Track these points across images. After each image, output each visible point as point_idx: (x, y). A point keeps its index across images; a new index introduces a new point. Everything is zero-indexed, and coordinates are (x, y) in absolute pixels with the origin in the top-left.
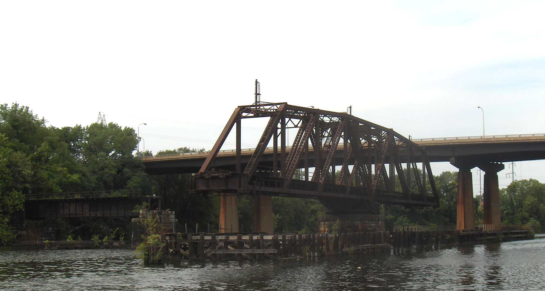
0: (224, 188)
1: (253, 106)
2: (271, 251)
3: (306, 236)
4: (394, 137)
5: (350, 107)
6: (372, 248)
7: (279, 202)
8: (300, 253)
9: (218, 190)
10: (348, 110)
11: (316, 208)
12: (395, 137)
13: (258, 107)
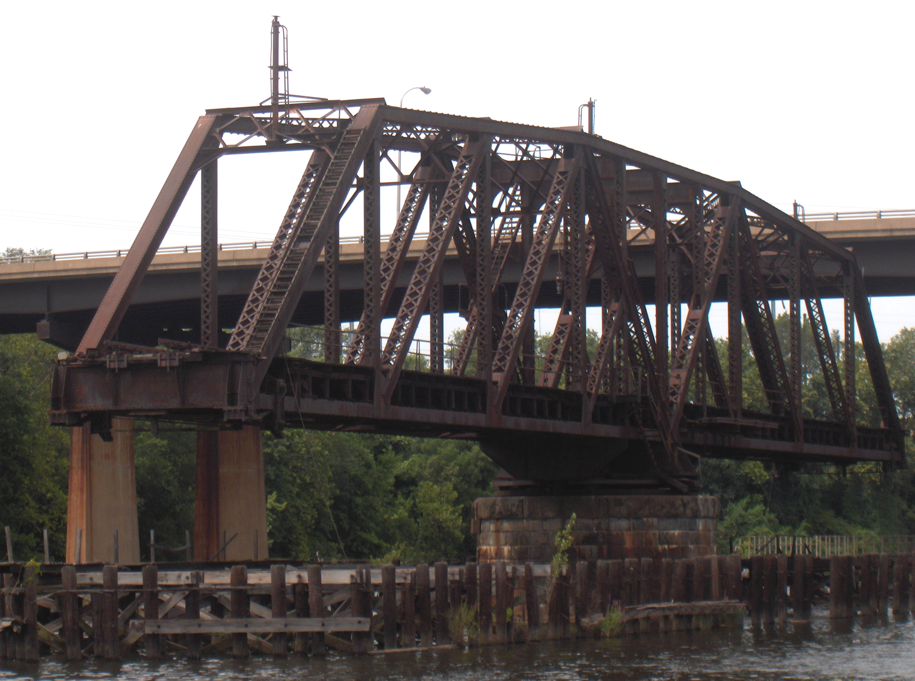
0: (175, 404)
1: (261, 109)
2: (350, 623)
3: (461, 573)
4: (746, 209)
5: (591, 105)
6: (678, 616)
7: (280, 447)
8: (442, 630)
9: (153, 410)
10: (580, 116)
11: (417, 469)
12: (749, 213)
13: (281, 114)
